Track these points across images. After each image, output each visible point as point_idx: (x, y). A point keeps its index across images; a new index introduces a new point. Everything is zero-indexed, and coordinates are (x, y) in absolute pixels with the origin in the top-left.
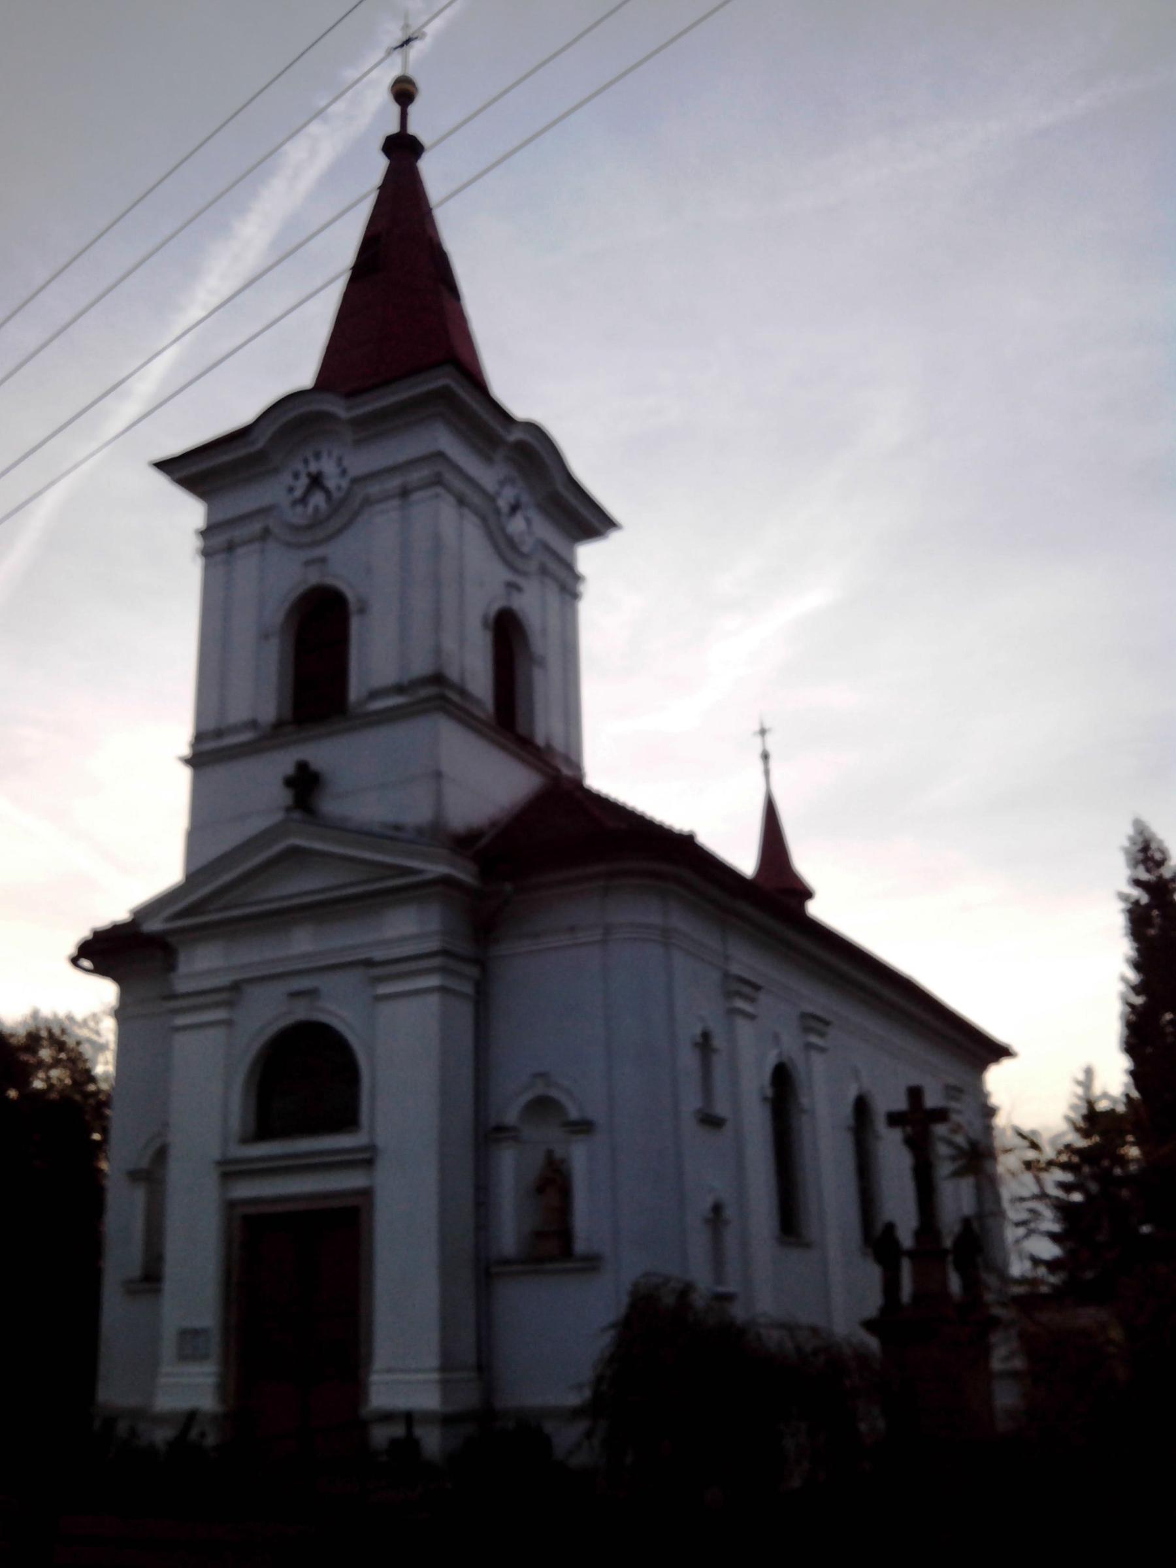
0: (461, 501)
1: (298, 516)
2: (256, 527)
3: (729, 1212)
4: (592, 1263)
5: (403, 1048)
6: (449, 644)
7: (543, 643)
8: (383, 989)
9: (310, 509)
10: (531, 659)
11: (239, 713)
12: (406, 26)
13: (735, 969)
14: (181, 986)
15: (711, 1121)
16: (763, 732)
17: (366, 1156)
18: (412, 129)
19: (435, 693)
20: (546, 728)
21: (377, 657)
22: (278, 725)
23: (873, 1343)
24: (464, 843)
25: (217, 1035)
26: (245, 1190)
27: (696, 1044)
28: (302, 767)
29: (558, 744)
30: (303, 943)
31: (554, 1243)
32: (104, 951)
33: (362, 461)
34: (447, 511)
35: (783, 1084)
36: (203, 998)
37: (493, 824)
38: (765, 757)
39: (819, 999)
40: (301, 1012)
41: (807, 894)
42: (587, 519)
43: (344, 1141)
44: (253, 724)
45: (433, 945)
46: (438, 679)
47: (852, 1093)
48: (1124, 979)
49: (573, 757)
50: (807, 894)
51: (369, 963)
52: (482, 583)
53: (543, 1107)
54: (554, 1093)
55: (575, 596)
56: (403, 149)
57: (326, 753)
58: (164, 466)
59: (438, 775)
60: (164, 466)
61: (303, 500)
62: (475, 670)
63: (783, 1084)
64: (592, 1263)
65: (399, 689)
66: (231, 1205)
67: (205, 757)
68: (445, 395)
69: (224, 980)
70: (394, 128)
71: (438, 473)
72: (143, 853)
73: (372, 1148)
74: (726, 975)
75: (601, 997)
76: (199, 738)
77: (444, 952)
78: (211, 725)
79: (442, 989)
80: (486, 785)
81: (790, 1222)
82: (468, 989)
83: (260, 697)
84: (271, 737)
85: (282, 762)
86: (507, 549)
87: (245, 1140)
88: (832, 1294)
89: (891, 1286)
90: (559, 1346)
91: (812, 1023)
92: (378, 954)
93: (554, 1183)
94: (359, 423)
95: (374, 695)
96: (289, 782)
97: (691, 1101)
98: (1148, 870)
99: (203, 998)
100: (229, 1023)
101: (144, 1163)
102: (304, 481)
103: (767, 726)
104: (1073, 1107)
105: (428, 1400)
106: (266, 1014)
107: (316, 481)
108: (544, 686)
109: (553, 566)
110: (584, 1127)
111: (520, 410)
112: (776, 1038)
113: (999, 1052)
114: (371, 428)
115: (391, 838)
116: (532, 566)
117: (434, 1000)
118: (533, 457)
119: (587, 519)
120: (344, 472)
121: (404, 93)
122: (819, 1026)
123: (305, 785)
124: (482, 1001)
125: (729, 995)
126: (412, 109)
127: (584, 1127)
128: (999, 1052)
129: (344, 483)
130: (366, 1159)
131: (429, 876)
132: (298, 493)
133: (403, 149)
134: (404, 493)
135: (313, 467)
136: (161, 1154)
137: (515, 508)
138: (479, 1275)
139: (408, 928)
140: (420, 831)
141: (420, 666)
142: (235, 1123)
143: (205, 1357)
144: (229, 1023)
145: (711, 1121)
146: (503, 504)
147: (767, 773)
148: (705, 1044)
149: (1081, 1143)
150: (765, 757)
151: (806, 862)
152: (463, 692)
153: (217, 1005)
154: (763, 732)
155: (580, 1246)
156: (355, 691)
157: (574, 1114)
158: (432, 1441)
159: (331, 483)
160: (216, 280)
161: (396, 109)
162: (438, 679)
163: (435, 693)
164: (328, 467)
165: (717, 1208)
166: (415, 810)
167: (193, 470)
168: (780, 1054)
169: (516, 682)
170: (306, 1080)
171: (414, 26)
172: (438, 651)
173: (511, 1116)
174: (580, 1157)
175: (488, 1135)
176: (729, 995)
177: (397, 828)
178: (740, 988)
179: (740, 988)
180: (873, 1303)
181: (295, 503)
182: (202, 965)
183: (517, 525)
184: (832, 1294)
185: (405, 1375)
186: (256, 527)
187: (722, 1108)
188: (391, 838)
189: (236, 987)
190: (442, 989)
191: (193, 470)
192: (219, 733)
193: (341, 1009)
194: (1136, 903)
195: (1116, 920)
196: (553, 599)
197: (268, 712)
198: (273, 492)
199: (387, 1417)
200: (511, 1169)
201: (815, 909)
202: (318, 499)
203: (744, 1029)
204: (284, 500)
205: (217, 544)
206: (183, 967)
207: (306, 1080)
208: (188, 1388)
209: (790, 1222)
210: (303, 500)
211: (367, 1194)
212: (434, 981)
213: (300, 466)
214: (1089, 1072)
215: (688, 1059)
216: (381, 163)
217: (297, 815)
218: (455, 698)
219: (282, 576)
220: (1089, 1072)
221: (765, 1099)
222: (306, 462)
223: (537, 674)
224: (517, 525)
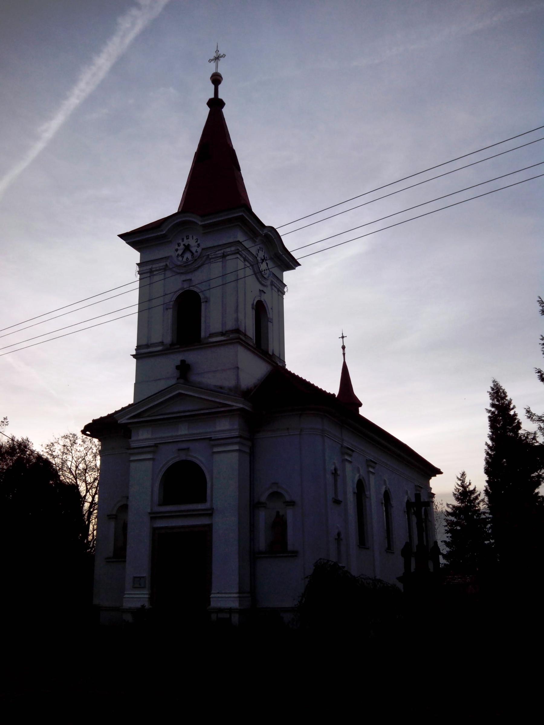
0: (245, 260)
1: (179, 261)
2: (162, 264)
3: (342, 536)
4: (294, 554)
5: (224, 472)
6: (241, 316)
7: (271, 314)
8: (216, 450)
9: (185, 259)
10: (268, 320)
11: (156, 338)
12: (217, 51)
13: (345, 444)
14: (133, 445)
15: (337, 502)
16: (343, 337)
17: (210, 512)
18: (220, 96)
19: (235, 336)
20: (272, 347)
21: (213, 320)
22: (172, 345)
23: (400, 586)
24: (246, 394)
25: (149, 464)
26: (160, 524)
27: (332, 473)
28: (183, 362)
29: (277, 354)
30: (183, 430)
31: (279, 546)
32: (94, 429)
33: (209, 243)
34: (241, 264)
35: (361, 488)
36: (141, 450)
37: (255, 387)
38: (344, 348)
39: (350, 441)
40: (183, 456)
41: (360, 405)
42: (291, 263)
43: (200, 506)
44: (162, 343)
45: (236, 434)
46: (237, 331)
47: (383, 490)
48: (486, 444)
49: (281, 358)
50: (360, 405)
51: (210, 439)
52: (251, 289)
53: (276, 495)
54: (280, 490)
55: (283, 293)
56: (216, 105)
57: (191, 356)
58: (122, 236)
59: (238, 368)
60: (122, 236)
61: (182, 255)
62: (249, 326)
63: (361, 488)
64: (294, 554)
65: (222, 334)
66: (155, 531)
67: (141, 355)
68: (241, 219)
69: (152, 443)
70: (212, 96)
71: (238, 249)
72: (118, 392)
73: (212, 509)
74: (342, 446)
75: (300, 455)
76: (138, 348)
77: (240, 437)
78: (144, 342)
79: (239, 451)
80: (252, 371)
81: (363, 541)
82: (247, 450)
83: (163, 333)
84: (168, 350)
85: (176, 359)
86: (259, 275)
87: (160, 505)
88: (386, 568)
89: (407, 565)
90: (286, 585)
91: (370, 463)
92: (213, 436)
93: (279, 525)
94: (205, 227)
95: (212, 335)
96: (177, 367)
97: (331, 495)
98: (498, 401)
99: (141, 450)
100: (153, 459)
101: (114, 512)
102: (182, 247)
103: (344, 335)
104: (457, 489)
105: (235, 604)
106: (169, 457)
107: (187, 248)
108: (272, 328)
109: (275, 281)
110: (292, 503)
111: (267, 223)
112: (359, 471)
113: (437, 472)
114: (209, 229)
115: (218, 392)
116: (268, 283)
117: (236, 454)
118: (270, 239)
119: (291, 263)
120: (199, 245)
121: (216, 80)
122: (373, 464)
123: (184, 369)
124: (252, 456)
125: (343, 454)
126: (220, 87)
127: (292, 503)
128: (437, 472)
129: (199, 250)
130: (210, 513)
131: (234, 408)
132: (180, 252)
133: (216, 105)
134: (224, 256)
135: (186, 242)
136: (124, 508)
137: (263, 260)
138: (252, 557)
139: (225, 426)
140: (230, 389)
141: (230, 326)
142: (156, 498)
143: (144, 587)
144: (153, 459)
145: (337, 502)
146: (259, 259)
147: (344, 354)
148: (335, 473)
149: (456, 503)
150: (344, 348)
151: (358, 391)
152: (245, 335)
153: (149, 452)
154: (343, 337)
155: (290, 548)
156: (203, 334)
157: (288, 498)
158: (235, 618)
159: (194, 250)
160: (75, 99)
161: (212, 87)
162: (237, 331)
163: (235, 336)
164: (192, 242)
165: (339, 534)
166: (226, 380)
167: (132, 238)
168: (360, 476)
169: (263, 330)
170: (184, 482)
171: (221, 53)
172: (237, 320)
173: (263, 499)
174: (290, 515)
175: (254, 505)
176: (343, 454)
177: (221, 388)
178: (346, 451)
179: (346, 451)
180: (401, 571)
181: (178, 256)
182: (143, 436)
183: (263, 266)
184: (386, 568)
185: (225, 595)
186: (162, 264)
187: (340, 498)
188: (218, 392)
189: (156, 446)
190: (239, 451)
191: (132, 238)
192: (147, 346)
193: (199, 456)
194: (493, 413)
195: (486, 423)
196: (275, 294)
197: (168, 340)
198: (168, 251)
199: (220, 610)
200: (263, 518)
201: (363, 412)
202: (188, 255)
203: (348, 466)
204: (174, 254)
205: (145, 269)
206: (134, 438)
207: (184, 482)
208: (137, 598)
209: (363, 541)
210: (182, 255)
211: (210, 526)
212: (236, 447)
213: (180, 241)
214: (463, 474)
215: (330, 478)
216: (207, 110)
217: (182, 381)
218: (243, 338)
219: (175, 284)
220: (463, 474)
221: (354, 493)
222: (183, 240)
223: (270, 324)
224: (263, 266)
